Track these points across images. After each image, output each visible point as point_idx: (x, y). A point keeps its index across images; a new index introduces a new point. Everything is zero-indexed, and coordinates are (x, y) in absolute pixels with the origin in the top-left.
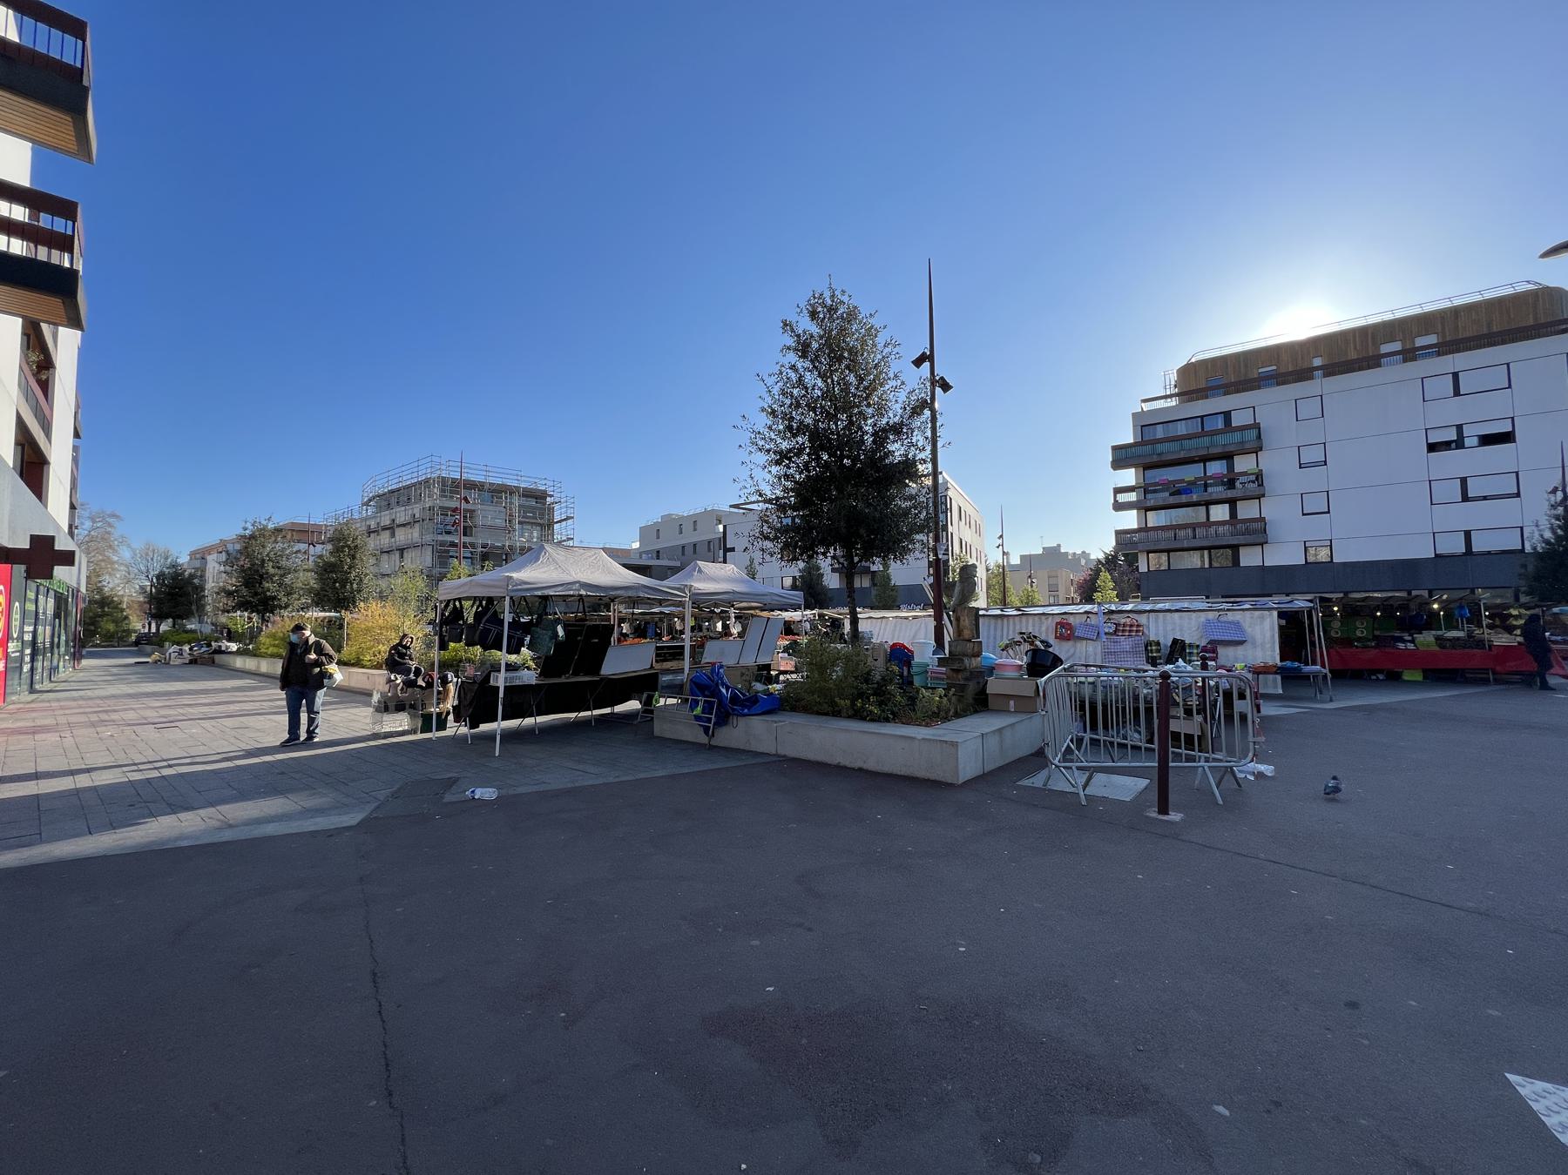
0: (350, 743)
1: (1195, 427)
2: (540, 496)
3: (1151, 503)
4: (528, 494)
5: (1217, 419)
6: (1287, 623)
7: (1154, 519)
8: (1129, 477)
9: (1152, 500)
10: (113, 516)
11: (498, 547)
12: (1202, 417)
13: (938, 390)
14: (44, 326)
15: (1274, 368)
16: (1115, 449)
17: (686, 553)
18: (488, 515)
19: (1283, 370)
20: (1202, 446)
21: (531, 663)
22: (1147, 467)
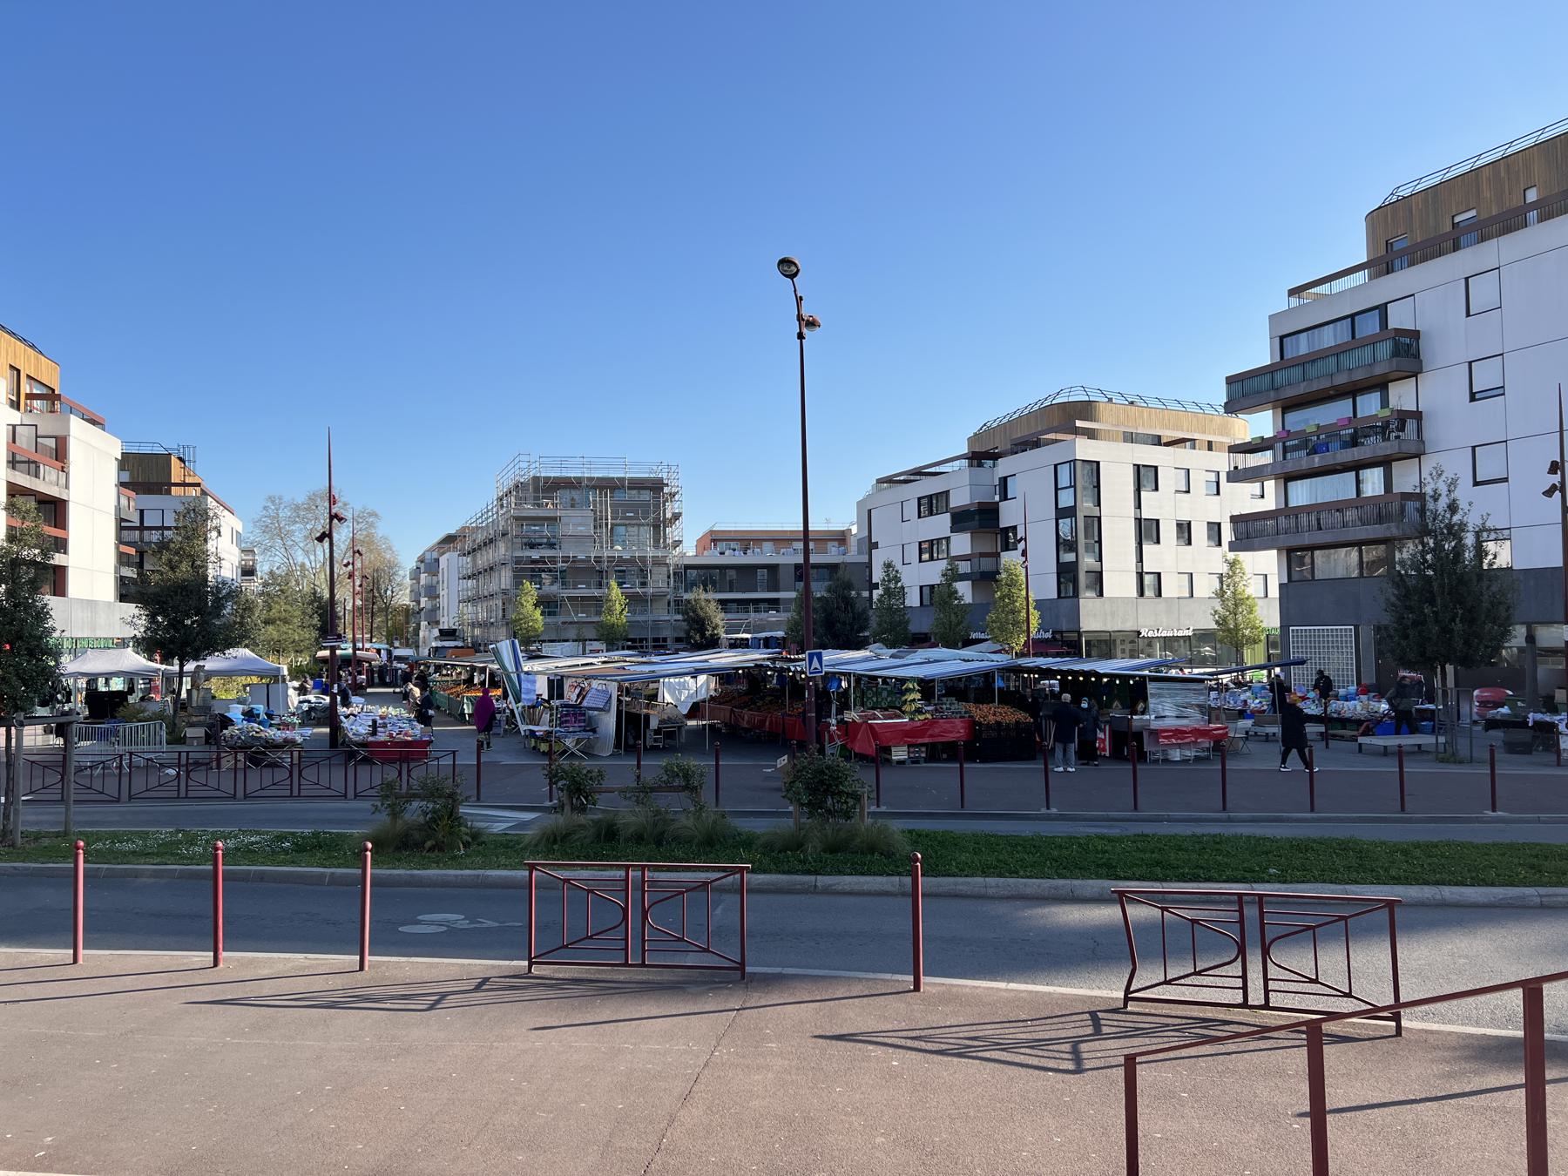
0: (954, 814)
1: (1340, 335)
2: (656, 486)
3: (1291, 467)
4: (638, 485)
5: (1298, 341)
6: (428, 712)
7: (1302, 494)
8: (1261, 424)
9: (1301, 460)
10: (371, 515)
11: (582, 561)
12: (1352, 316)
13: (335, 521)
14: (41, 466)
15: (1473, 213)
16: (1227, 378)
17: (1178, 495)
18: (575, 522)
19: (1484, 216)
20: (1357, 365)
21: (342, 718)
22: (1287, 406)
